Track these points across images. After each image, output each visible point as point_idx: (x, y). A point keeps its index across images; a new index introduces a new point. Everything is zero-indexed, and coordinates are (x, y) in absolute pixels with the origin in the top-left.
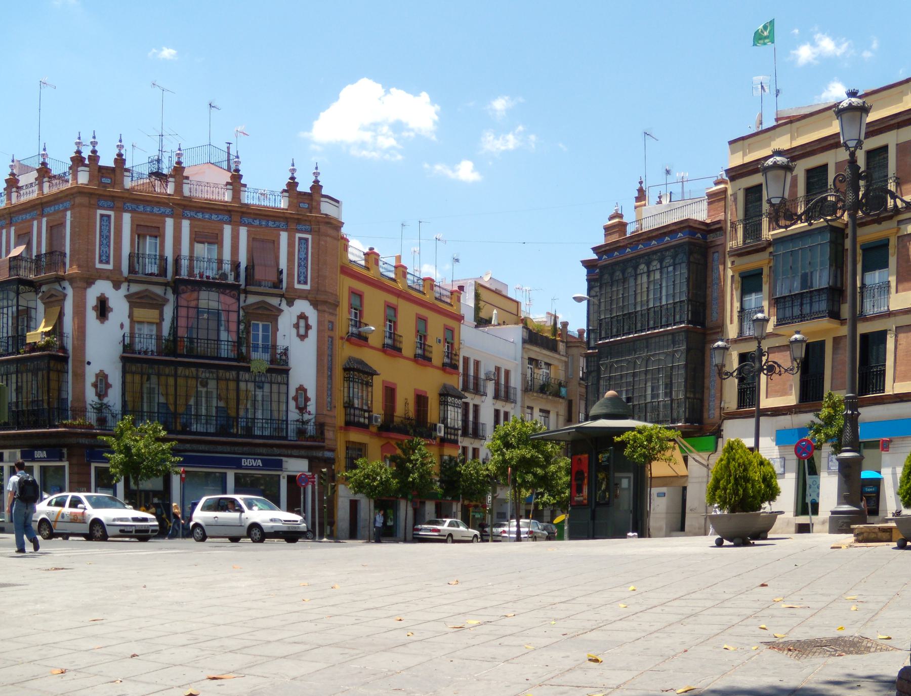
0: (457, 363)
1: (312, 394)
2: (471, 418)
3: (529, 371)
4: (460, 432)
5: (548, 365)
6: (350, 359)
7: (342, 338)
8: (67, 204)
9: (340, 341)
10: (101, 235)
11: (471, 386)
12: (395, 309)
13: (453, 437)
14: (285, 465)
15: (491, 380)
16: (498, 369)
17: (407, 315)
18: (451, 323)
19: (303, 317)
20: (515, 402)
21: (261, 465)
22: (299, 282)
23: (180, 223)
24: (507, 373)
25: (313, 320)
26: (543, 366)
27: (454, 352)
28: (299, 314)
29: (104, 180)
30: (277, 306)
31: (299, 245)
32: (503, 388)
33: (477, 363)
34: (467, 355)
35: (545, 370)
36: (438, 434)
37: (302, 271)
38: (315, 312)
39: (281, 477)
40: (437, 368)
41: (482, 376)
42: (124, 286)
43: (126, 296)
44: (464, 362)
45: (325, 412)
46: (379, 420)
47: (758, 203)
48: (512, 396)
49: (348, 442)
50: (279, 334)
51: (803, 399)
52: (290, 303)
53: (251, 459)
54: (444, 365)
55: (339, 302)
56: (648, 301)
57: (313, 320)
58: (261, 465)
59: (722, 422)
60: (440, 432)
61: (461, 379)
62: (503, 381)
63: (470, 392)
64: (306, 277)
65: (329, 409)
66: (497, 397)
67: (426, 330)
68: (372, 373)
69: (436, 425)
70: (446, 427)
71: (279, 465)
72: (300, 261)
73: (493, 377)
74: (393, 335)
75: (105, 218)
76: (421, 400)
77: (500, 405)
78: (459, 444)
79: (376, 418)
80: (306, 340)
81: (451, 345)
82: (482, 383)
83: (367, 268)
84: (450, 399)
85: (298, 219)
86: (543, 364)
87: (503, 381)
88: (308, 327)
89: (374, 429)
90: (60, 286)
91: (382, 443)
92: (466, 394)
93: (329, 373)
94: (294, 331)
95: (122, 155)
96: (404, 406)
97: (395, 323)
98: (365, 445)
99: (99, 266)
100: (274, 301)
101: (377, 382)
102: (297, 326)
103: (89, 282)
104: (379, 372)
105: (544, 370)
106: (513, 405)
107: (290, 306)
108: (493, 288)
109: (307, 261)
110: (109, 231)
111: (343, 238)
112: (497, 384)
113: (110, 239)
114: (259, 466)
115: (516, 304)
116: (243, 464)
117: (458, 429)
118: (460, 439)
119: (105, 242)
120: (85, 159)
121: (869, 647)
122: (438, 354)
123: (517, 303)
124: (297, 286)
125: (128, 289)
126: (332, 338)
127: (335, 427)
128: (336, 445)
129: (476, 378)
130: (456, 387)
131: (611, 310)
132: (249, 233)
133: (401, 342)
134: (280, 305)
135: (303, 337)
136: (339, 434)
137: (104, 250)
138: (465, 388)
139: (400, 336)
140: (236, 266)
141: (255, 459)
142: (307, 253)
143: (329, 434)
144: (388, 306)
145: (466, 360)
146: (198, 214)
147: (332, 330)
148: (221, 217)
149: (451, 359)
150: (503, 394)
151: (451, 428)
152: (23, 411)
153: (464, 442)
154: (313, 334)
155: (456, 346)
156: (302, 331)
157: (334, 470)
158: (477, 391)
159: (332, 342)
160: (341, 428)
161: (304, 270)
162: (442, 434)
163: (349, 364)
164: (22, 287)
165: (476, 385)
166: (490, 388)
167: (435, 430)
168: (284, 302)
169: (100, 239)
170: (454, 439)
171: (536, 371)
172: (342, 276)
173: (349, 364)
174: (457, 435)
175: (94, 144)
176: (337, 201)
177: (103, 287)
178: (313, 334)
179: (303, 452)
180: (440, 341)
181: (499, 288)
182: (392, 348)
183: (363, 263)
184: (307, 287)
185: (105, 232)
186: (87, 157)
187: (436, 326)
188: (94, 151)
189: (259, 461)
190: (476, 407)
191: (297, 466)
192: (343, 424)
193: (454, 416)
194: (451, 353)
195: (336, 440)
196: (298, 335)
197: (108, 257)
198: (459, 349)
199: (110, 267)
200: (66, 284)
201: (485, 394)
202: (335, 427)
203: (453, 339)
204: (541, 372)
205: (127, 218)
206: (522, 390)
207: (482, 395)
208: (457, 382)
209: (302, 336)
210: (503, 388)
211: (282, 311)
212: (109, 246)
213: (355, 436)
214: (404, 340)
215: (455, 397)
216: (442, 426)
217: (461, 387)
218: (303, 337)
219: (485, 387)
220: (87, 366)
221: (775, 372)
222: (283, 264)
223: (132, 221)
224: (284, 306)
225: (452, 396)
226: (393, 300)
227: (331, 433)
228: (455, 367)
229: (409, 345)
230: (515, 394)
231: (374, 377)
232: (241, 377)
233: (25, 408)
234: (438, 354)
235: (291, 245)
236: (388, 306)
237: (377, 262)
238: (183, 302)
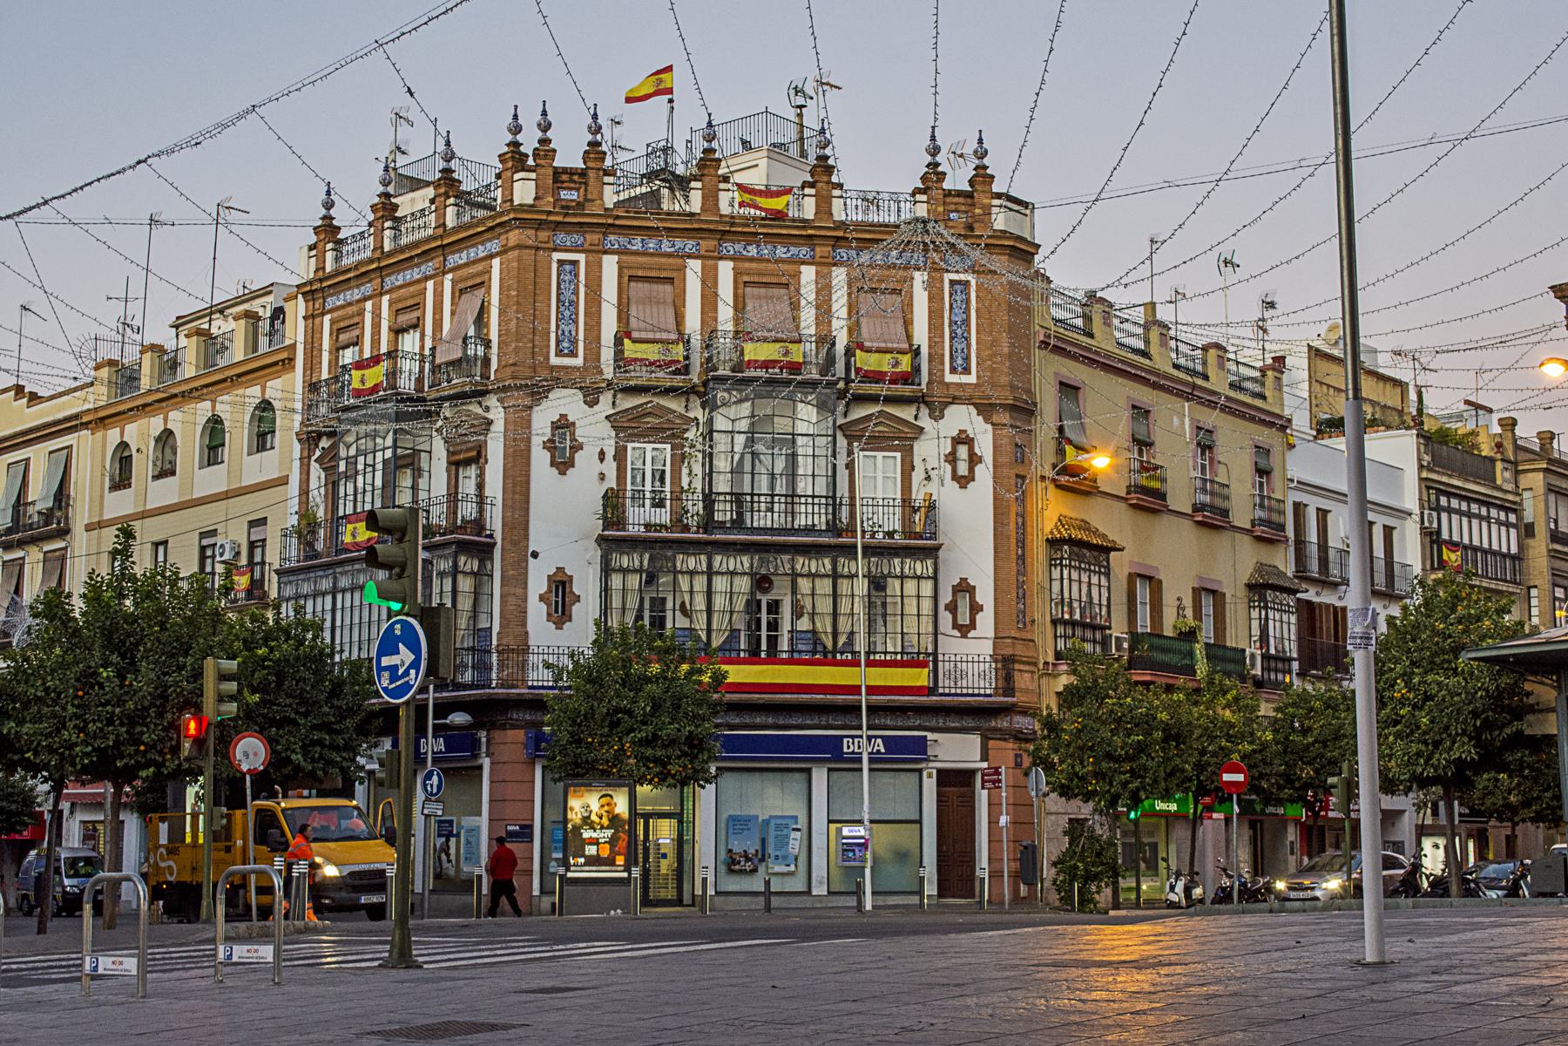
1: (985, 596)
8: (494, 246)
10: (558, 300)
18: (1265, 436)
19: (963, 439)
21: (883, 750)
22: (559, 353)
23: (716, 268)
25: (985, 446)
29: (564, 194)
31: (559, 275)
32: (1313, 550)
37: (567, 329)
38: (989, 427)
42: (606, 399)
52: (937, 414)
57: (985, 446)
58: (883, 750)
64: (967, 359)
72: (955, 327)
75: (568, 267)
88: (974, 460)
90: (480, 403)
95: (986, 168)
99: (555, 360)
100: (906, 413)
101: (1120, 565)
102: (952, 458)
103: (538, 393)
109: (969, 326)
110: (576, 292)
113: (577, 308)
114: (878, 751)
116: (845, 750)
119: (567, 313)
120: (527, 156)
124: (950, 378)
125: (614, 403)
132: (737, 273)
134: (916, 417)
135: (964, 481)
137: (959, 347)
142: (967, 311)
146: (749, 248)
148: (794, 250)
154: (984, 473)
156: (963, 469)
161: (964, 345)
163: (1060, 532)
168: (924, 411)
169: (558, 307)
173: (1060, 532)
174: (1290, 672)
175: (545, 127)
176: (1025, 204)
177: (565, 402)
178: (984, 473)
179: (969, 722)
184: (972, 379)
185: (568, 296)
188: (544, 141)
196: (955, 477)
197: (574, 342)
199: (578, 361)
200: (492, 401)
205: (610, 264)
210: (1313, 550)
212: (576, 322)
218: (964, 481)
220: (531, 560)
222: (921, 336)
223: (620, 269)
224: (925, 421)
226: (1144, 395)
231: (1112, 554)
232: (840, 569)
235: (934, 298)
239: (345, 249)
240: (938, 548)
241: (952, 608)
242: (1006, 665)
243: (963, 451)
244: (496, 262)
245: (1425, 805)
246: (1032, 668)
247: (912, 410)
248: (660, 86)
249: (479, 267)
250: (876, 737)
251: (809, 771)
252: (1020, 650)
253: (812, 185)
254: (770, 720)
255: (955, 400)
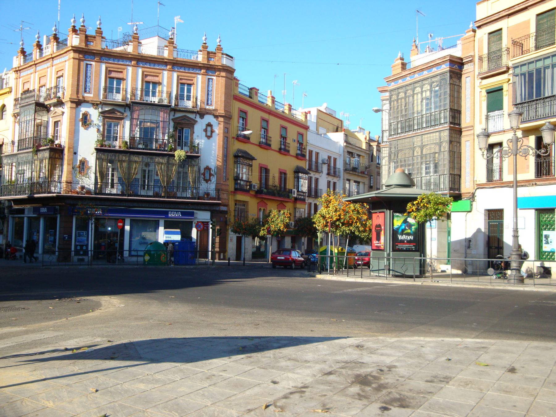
0: (305, 154)
2: (313, 186)
3: (348, 159)
4: (307, 194)
5: (359, 156)
6: (239, 151)
7: (233, 138)
9: (232, 139)
11: (314, 167)
12: (267, 121)
13: (302, 197)
14: (195, 215)
15: (325, 164)
16: (329, 158)
17: (275, 125)
18: (302, 130)
19: (209, 125)
20: (339, 177)
24: (335, 160)
26: (356, 156)
27: (303, 147)
28: (207, 123)
30: (194, 118)
32: (314, 163)
33: (317, 154)
34: (311, 149)
35: (357, 159)
36: (293, 196)
39: (193, 223)
40: (293, 156)
41: (320, 161)
43: (101, 113)
44: (309, 153)
45: (222, 182)
46: (256, 187)
47: (499, 42)
48: (337, 173)
49: (236, 201)
50: (195, 136)
51: (538, 176)
53: (175, 211)
54: (297, 154)
55: (232, 116)
56: (422, 111)
59: (476, 190)
60: (294, 194)
61: (307, 163)
62: (332, 165)
63: (313, 171)
65: (224, 180)
66: (328, 174)
67: (286, 135)
68: (252, 159)
69: (291, 190)
70: (298, 191)
71: (192, 214)
73: (326, 162)
74: (266, 137)
76: (283, 174)
77: (330, 179)
78: (306, 201)
79: (254, 186)
80: (211, 139)
81: (301, 144)
82: (320, 165)
83: (250, 97)
84: (300, 175)
85: (208, 67)
86: (356, 155)
87: (332, 165)
89: (252, 193)
91: (258, 201)
92: (310, 172)
93: (225, 159)
94: (204, 133)
96: (274, 179)
97: (267, 130)
98: (246, 202)
101: (255, 164)
102: (206, 130)
104: (256, 158)
105: (357, 159)
106: (338, 179)
107: (202, 119)
108: (328, 112)
111: (235, 79)
112: (329, 166)
115: (341, 122)
117: (305, 193)
118: (307, 198)
121: (419, 209)
122: (293, 148)
123: (341, 121)
126: (227, 137)
127: (228, 191)
128: (229, 202)
129: (317, 162)
130: (304, 167)
131: (398, 117)
133: (289, 147)
136: (230, 196)
138: (310, 169)
139: (270, 137)
140: (170, 95)
141: (177, 212)
143: (224, 196)
144: (263, 119)
145: (311, 152)
147: (227, 133)
149: (302, 151)
150: (333, 172)
151: (301, 192)
152: (34, 183)
153: (308, 200)
155: (304, 144)
156: (209, 134)
157: (226, 218)
158: (317, 171)
159: (227, 140)
160: (232, 192)
162: (296, 196)
164: (39, 108)
165: (317, 166)
166: (325, 168)
167: (291, 193)
168: (198, 116)
170: (303, 199)
171: (352, 159)
172: (234, 101)
174: (305, 196)
176: (232, 57)
179: (207, 208)
180: (295, 141)
181: (331, 113)
182: (266, 145)
183: (248, 94)
186: (78, 29)
187: (292, 132)
189: (180, 213)
190: (317, 180)
191: (204, 216)
192: (233, 190)
193: (304, 185)
194: (302, 148)
195: (228, 200)
196: (207, 136)
198: (306, 145)
201: (322, 172)
202: (228, 191)
203: (303, 141)
204: (354, 159)
206: (343, 170)
207: (320, 173)
208: (304, 165)
209: (209, 136)
210: (314, 163)
211: (197, 121)
213: (240, 197)
214: (272, 139)
215: (304, 173)
216: (296, 190)
217: (307, 168)
218: (209, 137)
219: (322, 167)
221: (529, 154)
225: (302, 173)
226: (266, 116)
227: (225, 195)
228: (304, 156)
229: (275, 143)
230: (339, 172)
231: (253, 161)
233: (35, 181)
234: (293, 148)
236: (263, 119)
237: (256, 94)
238: (135, 116)
239: (27, 58)
240: (198, 157)
241: (204, 174)
242: (218, 190)
243: (209, 129)
244: (67, 63)
245: (77, 252)
246: (227, 193)
247: (194, 115)
248: (509, 257)
249: (62, 64)
250: (179, 211)
251: (124, 220)
252: (223, 187)
253: (167, 47)
254: (147, 206)
255: (207, 113)
